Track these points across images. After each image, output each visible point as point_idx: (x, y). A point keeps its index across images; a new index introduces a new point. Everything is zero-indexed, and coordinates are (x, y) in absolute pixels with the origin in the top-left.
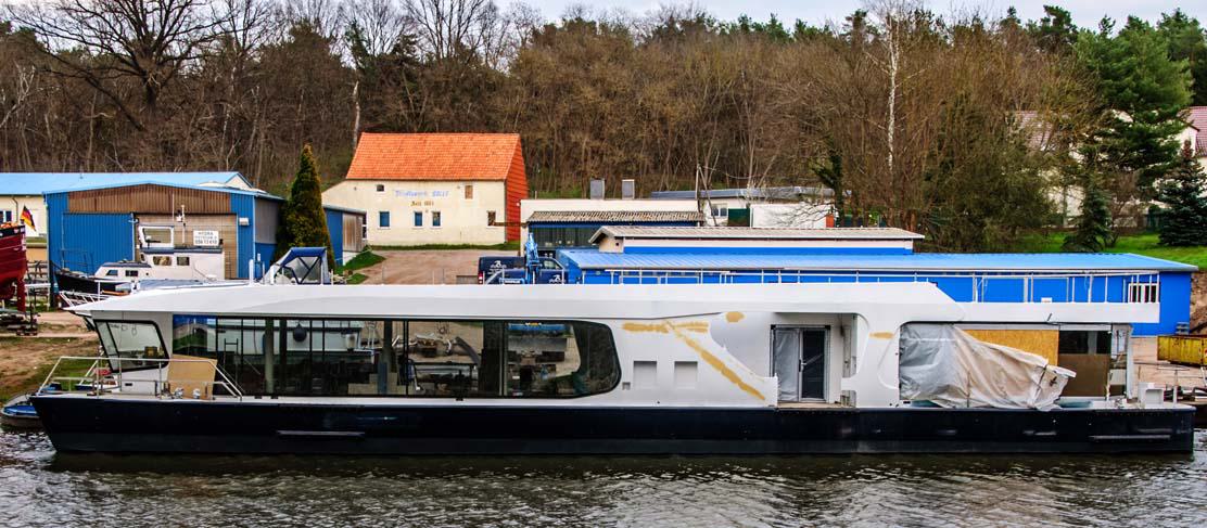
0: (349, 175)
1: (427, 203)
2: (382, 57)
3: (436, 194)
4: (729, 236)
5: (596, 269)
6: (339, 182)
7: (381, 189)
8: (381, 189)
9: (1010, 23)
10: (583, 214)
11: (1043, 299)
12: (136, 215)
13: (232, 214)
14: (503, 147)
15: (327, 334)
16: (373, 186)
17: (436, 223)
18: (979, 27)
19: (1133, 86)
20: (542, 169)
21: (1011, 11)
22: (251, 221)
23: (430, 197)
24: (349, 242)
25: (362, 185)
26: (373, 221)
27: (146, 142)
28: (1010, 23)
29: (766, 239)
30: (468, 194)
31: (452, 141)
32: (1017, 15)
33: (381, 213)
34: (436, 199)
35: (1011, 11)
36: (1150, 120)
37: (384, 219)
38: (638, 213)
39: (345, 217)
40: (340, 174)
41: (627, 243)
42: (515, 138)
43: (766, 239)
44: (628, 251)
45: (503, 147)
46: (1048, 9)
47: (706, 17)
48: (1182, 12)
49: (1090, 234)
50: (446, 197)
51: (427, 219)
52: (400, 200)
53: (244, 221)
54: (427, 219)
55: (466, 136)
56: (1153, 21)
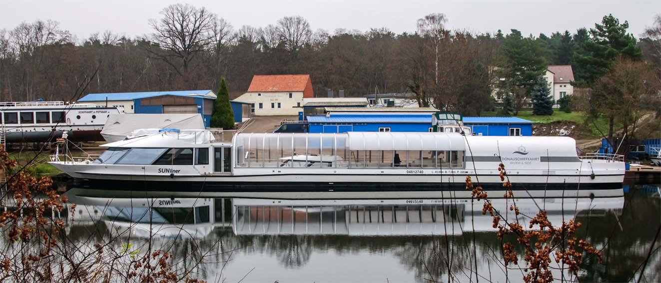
0: (249, 90)
1: (276, 100)
2: (274, 49)
3: (279, 96)
4: (419, 111)
5: (320, 123)
6: (244, 93)
7: (260, 95)
8: (260, 95)
9: (499, 35)
10: (325, 103)
11: (479, 134)
12: (163, 106)
13: (195, 105)
14: (303, 80)
15: (441, 197)
16: (257, 94)
17: (279, 107)
18: (488, 36)
19: (601, 55)
20: (319, 88)
21: (499, 31)
22: (202, 107)
23: (277, 98)
24: (245, 114)
25: (252, 94)
26: (257, 107)
27: (549, 53)
28: (499, 35)
29: (408, 112)
30: (291, 96)
31: (285, 78)
32: (502, 33)
33: (541, 161)
34: (279, 98)
35: (499, 31)
36: (534, 70)
37: (261, 105)
38: (345, 103)
39: (243, 105)
40: (244, 90)
41: (331, 113)
42: (308, 76)
43: (408, 112)
44: (332, 116)
45: (303, 80)
46: (512, 30)
47: (392, 33)
48: (559, 32)
49: (508, 109)
50: (283, 98)
51: (276, 105)
52: (266, 99)
53: (200, 107)
54: (276, 105)
55: (290, 76)
56: (549, 35)
